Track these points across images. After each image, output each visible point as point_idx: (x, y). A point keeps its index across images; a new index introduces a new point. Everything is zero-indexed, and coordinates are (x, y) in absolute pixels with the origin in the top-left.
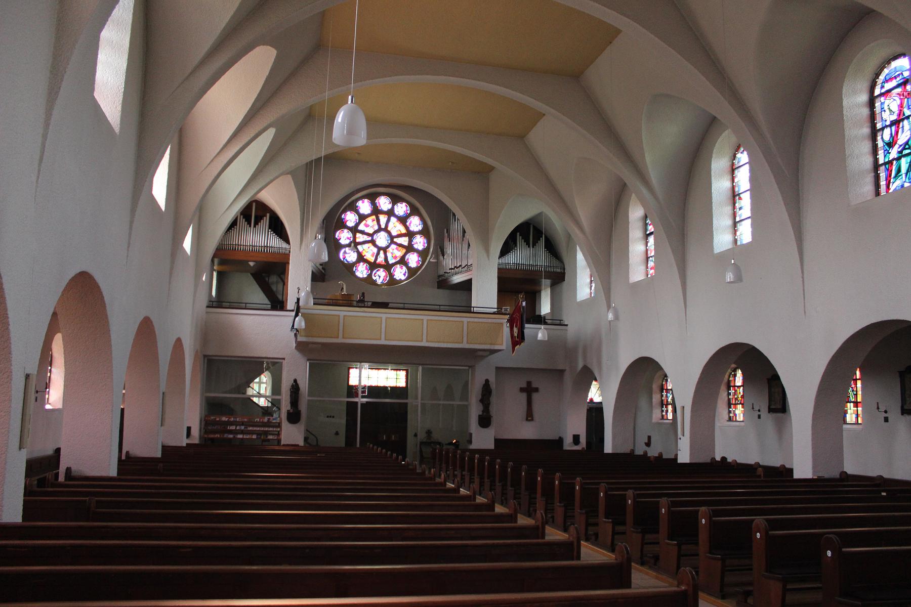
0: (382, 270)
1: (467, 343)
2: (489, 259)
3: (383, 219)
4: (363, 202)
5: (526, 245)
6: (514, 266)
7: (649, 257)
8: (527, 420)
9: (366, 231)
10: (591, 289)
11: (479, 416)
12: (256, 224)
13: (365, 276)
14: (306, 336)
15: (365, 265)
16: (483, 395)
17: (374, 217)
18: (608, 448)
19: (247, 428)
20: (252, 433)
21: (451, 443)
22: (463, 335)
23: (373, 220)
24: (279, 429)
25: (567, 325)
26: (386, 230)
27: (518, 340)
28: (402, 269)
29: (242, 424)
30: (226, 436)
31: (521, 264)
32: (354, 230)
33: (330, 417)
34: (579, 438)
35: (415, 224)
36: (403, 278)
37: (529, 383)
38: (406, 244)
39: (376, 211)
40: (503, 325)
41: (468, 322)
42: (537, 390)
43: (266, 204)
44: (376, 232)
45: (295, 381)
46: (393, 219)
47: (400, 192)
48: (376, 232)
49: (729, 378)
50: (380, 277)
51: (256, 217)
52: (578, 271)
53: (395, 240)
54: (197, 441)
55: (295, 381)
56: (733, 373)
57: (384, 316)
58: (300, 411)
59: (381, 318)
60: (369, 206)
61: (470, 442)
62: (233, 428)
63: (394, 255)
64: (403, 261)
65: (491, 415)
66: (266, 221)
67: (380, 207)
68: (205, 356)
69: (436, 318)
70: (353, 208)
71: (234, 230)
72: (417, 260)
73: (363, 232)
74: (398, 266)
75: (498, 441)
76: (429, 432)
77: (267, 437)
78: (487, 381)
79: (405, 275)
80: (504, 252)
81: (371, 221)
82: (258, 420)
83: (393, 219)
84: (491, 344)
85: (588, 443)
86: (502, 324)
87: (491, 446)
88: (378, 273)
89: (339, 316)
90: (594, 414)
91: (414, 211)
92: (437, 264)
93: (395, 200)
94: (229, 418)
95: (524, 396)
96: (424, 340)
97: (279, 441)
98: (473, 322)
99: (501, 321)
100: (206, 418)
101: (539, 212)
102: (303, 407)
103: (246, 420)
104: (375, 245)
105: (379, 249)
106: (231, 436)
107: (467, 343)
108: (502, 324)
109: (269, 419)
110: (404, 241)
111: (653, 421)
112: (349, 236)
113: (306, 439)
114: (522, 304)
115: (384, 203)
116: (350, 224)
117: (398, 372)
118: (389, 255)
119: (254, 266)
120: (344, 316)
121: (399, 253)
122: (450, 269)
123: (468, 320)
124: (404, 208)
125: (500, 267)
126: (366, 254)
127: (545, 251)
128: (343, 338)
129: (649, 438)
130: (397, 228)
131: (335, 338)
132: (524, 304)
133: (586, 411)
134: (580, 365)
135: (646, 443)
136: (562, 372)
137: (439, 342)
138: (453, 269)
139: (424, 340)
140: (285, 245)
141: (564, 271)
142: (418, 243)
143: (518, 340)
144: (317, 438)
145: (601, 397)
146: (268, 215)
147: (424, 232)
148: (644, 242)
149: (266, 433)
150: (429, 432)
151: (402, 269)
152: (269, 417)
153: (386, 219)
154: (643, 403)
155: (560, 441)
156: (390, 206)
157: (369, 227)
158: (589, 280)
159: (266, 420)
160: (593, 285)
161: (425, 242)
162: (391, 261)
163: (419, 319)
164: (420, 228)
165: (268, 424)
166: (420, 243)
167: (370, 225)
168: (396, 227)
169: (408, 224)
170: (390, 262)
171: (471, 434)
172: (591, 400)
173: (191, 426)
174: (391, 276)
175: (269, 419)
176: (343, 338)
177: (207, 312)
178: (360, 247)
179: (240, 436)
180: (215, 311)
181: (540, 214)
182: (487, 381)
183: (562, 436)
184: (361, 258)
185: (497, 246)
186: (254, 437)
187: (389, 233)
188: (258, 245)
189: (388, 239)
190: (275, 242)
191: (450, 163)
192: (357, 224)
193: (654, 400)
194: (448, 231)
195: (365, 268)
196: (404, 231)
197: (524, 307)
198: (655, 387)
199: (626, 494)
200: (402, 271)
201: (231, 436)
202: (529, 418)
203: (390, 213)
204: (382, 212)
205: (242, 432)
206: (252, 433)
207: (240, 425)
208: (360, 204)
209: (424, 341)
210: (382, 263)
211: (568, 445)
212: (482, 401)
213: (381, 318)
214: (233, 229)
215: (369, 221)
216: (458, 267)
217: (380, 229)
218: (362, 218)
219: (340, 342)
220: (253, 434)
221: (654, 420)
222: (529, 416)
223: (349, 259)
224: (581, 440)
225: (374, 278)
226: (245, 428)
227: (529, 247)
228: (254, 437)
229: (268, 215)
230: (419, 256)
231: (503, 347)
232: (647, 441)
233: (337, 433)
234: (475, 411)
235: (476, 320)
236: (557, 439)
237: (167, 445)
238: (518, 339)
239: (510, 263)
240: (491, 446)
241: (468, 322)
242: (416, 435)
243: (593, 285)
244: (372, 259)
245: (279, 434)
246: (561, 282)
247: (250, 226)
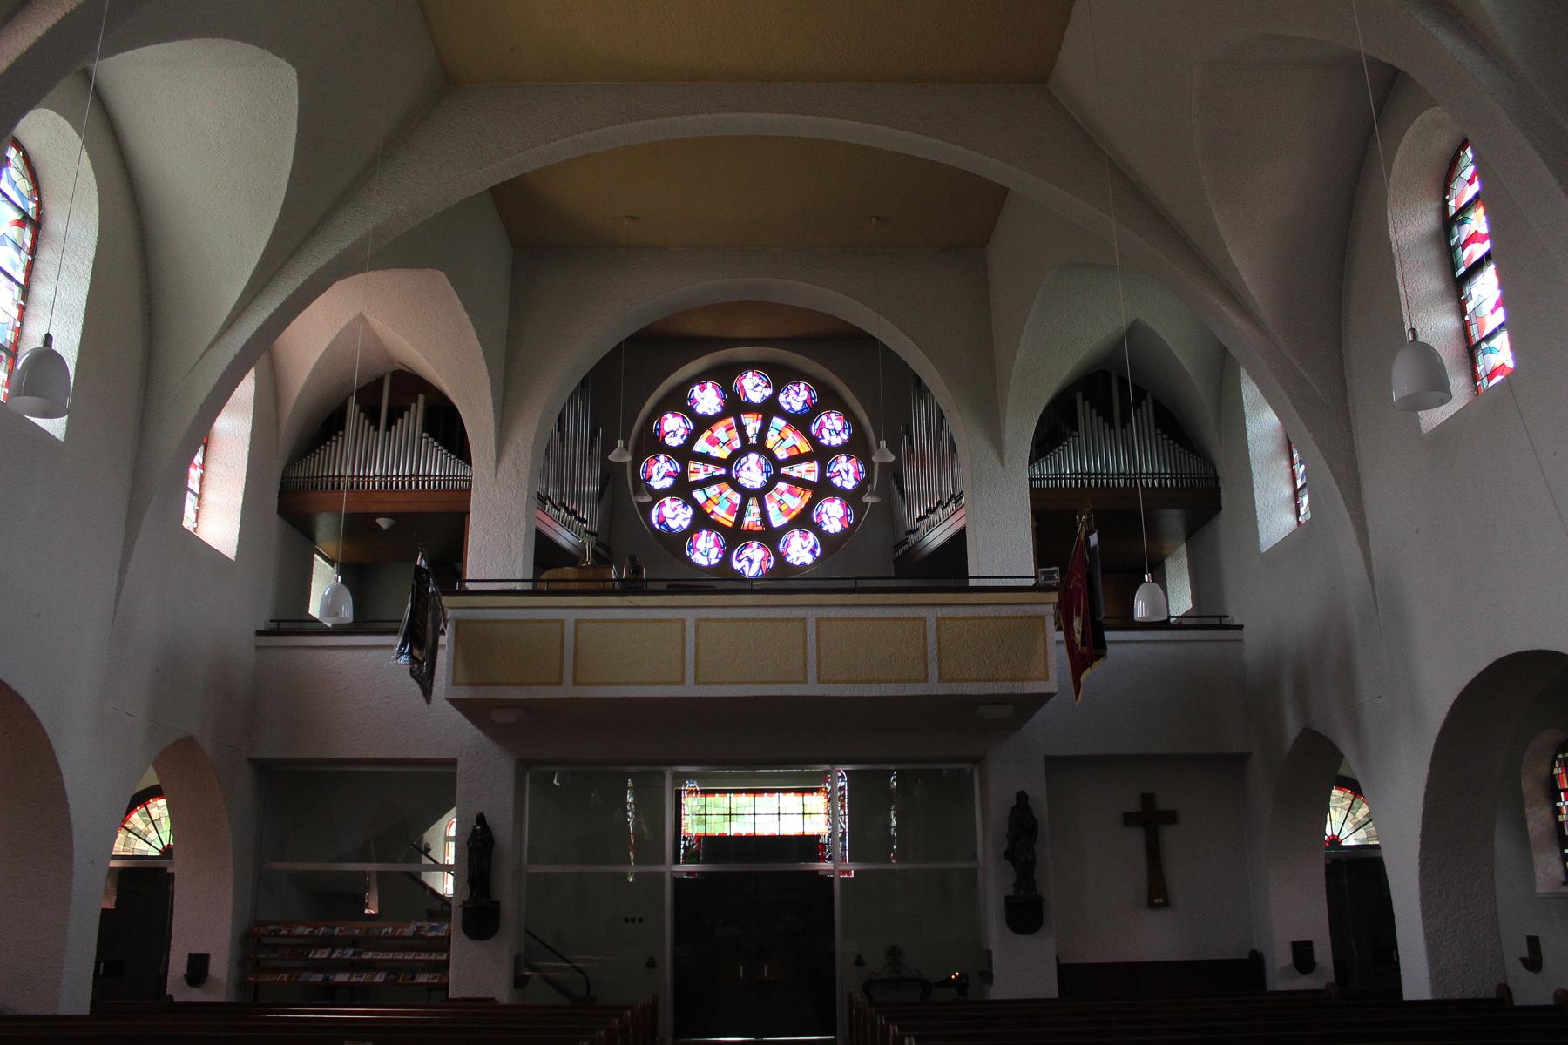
0: (755, 545)
1: (941, 679)
2: (1003, 464)
3: (752, 424)
4: (703, 389)
5: (1104, 422)
6: (1076, 480)
7: (1479, 343)
8: (1152, 905)
9: (712, 454)
10: (1298, 514)
11: (1007, 898)
12: (391, 422)
13: (714, 562)
14: (471, 684)
15: (713, 535)
16: (1013, 839)
17: (732, 420)
18: (1416, 982)
19: (360, 954)
20: (371, 966)
21: (947, 982)
22: (925, 657)
23: (729, 429)
24: (444, 957)
25: (1240, 627)
26: (761, 447)
27: (1085, 650)
28: (805, 538)
29: (354, 942)
30: (304, 977)
31: (1095, 474)
32: (684, 454)
33: (633, 920)
34: (1311, 952)
35: (833, 429)
36: (809, 560)
37: (1148, 799)
38: (813, 477)
39: (735, 406)
40: (1044, 622)
41: (938, 619)
42: (1171, 817)
43: (427, 378)
44: (736, 455)
45: (481, 819)
46: (778, 423)
47: (785, 352)
48: (736, 455)
49: (1552, 770)
50: (751, 561)
51: (390, 409)
52: (1255, 468)
53: (785, 470)
54: (220, 996)
55: (481, 819)
56: (1560, 756)
57: (690, 616)
58: (498, 903)
59: (683, 621)
60: (718, 395)
61: (988, 977)
62: (322, 954)
63: (784, 508)
64: (804, 521)
65: (1040, 897)
66: (416, 414)
67: (745, 395)
68: (266, 771)
69: (846, 612)
70: (679, 402)
71: (337, 441)
72: (841, 513)
73: (705, 458)
74: (797, 532)
75: (1068, 974)
76: (894, 954)
77: (413, 978)
78: (1022, 797)
79: (813, 552)
80: (1046, 442)
81: (724, 430)
82: (390, 930)
83: (778, 423)
84: (1013, 679)
85: (1339, 964)
86: (1041, 619)
87: (1048, 988)
88: (748, 552)
89: (562, 622)
90: (1345, 881)
91: (826, 400)
92: (888, 512)
93: (780, 377)
94: (316, 928)
95: (1137, 836)
96: (812, 676)
97: (445, 987)
98: (951, 618)
99: (1039, 610)
100: (255, 929)
101: (1123, 323)
102: (507, 892)
103: (357, 931)
104: (736, 486)
105: (747, 493)
106: (319, 978)
107: (941, 679)
108: (1041, 619)
109: (419, 928)
110: (808, 471)
111: (1540, 890)
112: (672, 470)
113: (519, 982)
114: (1088, 541)
115: (754, 387)
116: (673, 441)
117: (807, 797)
118: (772, 508)
119: (390, 528)
120: (577, 622)
121: (796, 503)
122: (918, 520)
123: (939, 615)
124: (804, 395)
125: (1036, 484)
126: (716, 509)
127: (1156, 435)
128: (575, 683)
129: (1533, 942)
130: (789, 442)
131: (551, 684)
132: (1094, 539)
133: (1323, 870)
134: (1292, 730)
135: (1523, 960)
136: (1236, 763)
137: (855, 682)
138: (924, 517)
139: (812, 676)
140: (459, 469)
141: (1217, 483)
142: (844, 474)
143: (1085, 650)
144: (587, 979)
145: (1501, 311)
146: (421, 398)
147: (856, 447)
148: (1451, 304)
149: (414, 968)
150: (894, 954)
151: (805, 538)
152: (419, 924)
153: (759, 424)
154: (1503, 844)
155: (1254, 964)
156: (768, 392)
157: (721, 444)
158: (1288, 491)
159: (409, 930)
160: (1305, 500)
161: (861, 470)
162: (777, 520)
163: (794, 620)
164: (844, 436)
165: (419, 942)
166: (846, 472)
167: (719, 442)
168: (785, 441)
169: (814, 429)
170: (775, 524)
171: (989, 953)
172: (1335, 841)
173: (211, 952)
174: (780, 558)
175: (419, 928)
176: (575, 683)
177: (257, 648)
178: (699, 495)
179: (342, 978)
180: (302, 644)
181: (1134, 328)
182: (1022, 797)
183: (1256, 947)
184: (702, 520)
185: (1021, 430)
186: (379, 978)
187: (769, 455)
188: (395, 474)
189: (768, 469)
190: (436, 465)
191: (874, 220)
192: (692, 437)
193: (1531, 825)
194: (908, 432)
195: (712, 544)
196: (805, 448)
197: (1095, 547)
198: (1529, 785)
199: (880, 463)
200: (805, 543)
201: (319, 978)
202: (1156, 901)
203: (769, 409)
204: (751, 408)
205: (354, 966)
206: (371, 966)
207: (344, 947)
208: (696, 392)
209: (809, 679)
210: (755, 529)
211: (1280, 976)
212: (1009, 855)
213: (683, 621)
214: (328, 443)
215: (720, 432)
216: (935, 509)
217: (746, 449)
218: (702, 423)
219: (562, 695)
220: (379, 969)
221: (1541, 888)
222: (1158, 894)
223: (673, 524)
224: (1317, 958)
225: (737, 566)
226: (354, 954)
227: (1112, 426)
228: (379, 978)
229: (421, 398)
230: (847, 506)
231: (1050, 686)
232: (1526, 954)
233: (651, 964)
234: (995, 886)
235: (961, 612)
236: (1246, 956)
237: (9, 1013)
238: (1087, 652)
239: (1065, 474)
240: (1048, 988)
241: (938, 619)
242: (859, 962)
243: (1305, 500)
244: (729, 520)
245: (444, 966)
246: (1217, 513)
247: (377, 429)
